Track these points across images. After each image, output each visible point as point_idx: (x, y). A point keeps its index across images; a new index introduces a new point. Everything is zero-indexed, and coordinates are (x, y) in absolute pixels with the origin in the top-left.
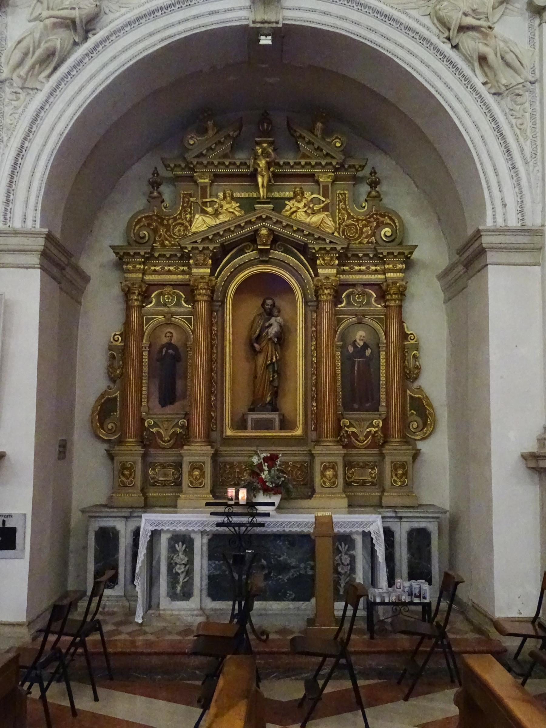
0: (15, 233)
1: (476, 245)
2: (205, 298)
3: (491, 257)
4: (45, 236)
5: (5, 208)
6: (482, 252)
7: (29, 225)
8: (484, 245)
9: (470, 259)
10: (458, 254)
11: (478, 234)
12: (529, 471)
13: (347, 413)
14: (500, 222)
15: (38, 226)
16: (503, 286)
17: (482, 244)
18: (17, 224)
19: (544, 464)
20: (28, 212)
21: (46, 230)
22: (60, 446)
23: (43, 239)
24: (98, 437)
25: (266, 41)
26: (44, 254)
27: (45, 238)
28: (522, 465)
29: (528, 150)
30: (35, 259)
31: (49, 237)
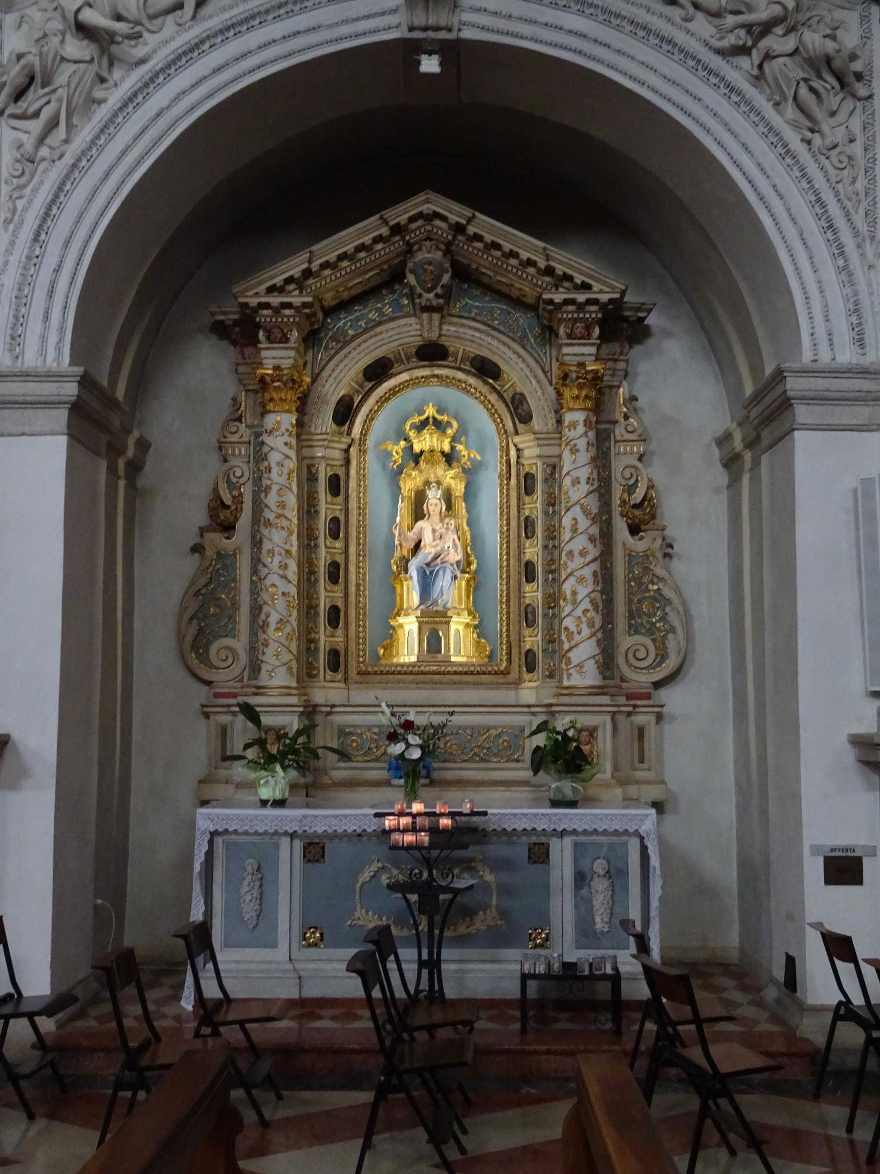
0: (26, 376)
1: (779, 390)
2: (339, 507)
3: (802, 413)
4: (78, 379)
5: (268, 801)
6: (785, 404)
7: (51, 363)
8: (790, 394)
9: (766, 418)
10: (745, 408)
11: (779, 376)
12: (865, 768)
13: (645, 691)
14: (825, 357)
15: (66, 359)
16: (823, 465)
17: (786, 391)
18: (30, 360)
19: (879, 756)
20: (48, 345)
21: (79, 370)
22: (92, 967)
23: (76, 384)
24: (183, 659)
25: (430, 65)
26: (77, 409)
27: (79, 382)
28: (850, 756)
29: (859, 220)
30: (61, 416)
31: (86, 382)
